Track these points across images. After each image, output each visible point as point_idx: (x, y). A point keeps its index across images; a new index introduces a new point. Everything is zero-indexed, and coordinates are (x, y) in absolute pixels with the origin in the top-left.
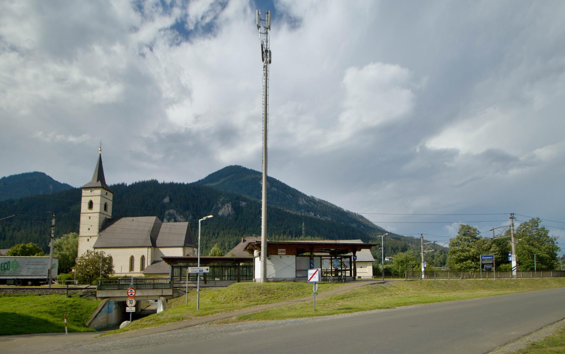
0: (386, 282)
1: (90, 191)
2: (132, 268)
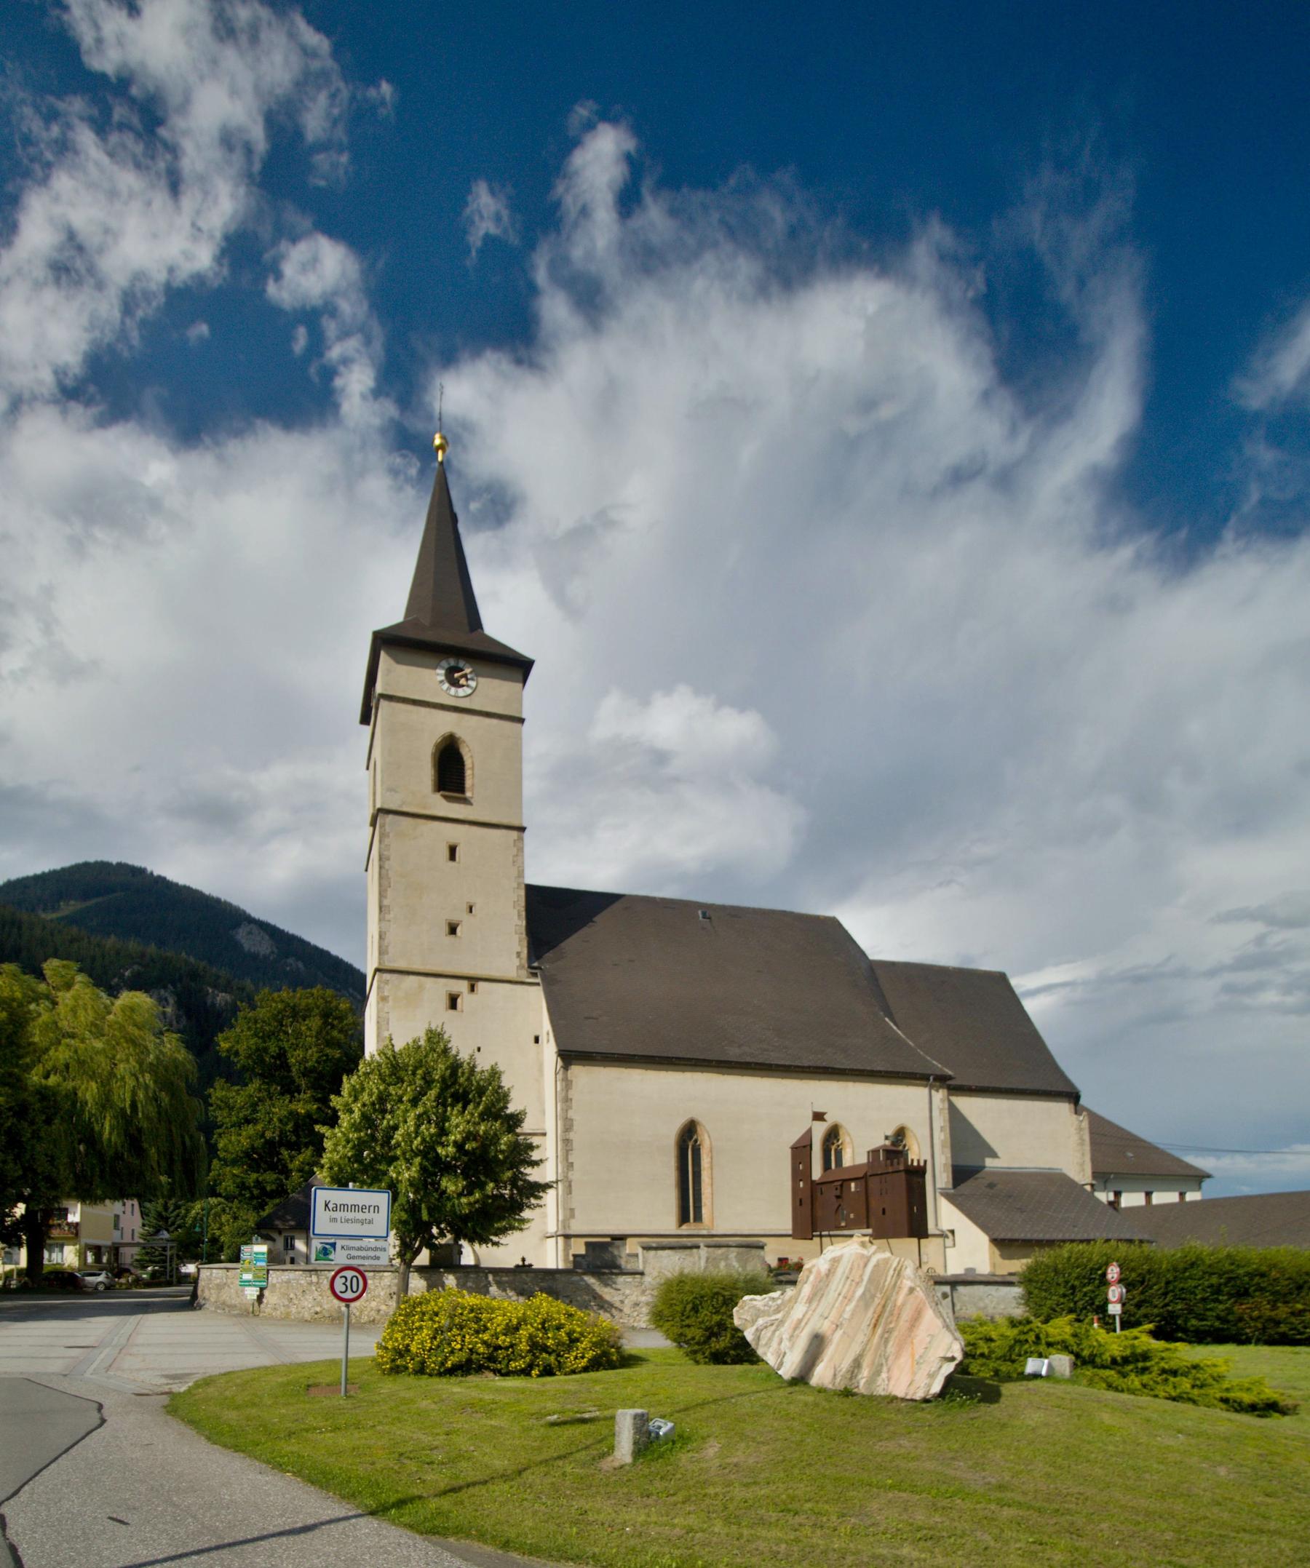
0: (901, 1270)
1: (440, 674)
2: (133, 1238)
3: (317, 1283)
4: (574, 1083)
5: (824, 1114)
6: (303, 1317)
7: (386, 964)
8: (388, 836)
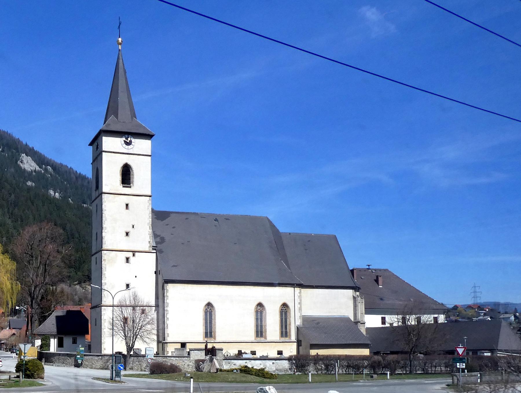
4: (169, 290)
7: (105, 248)
8: (106, 202)
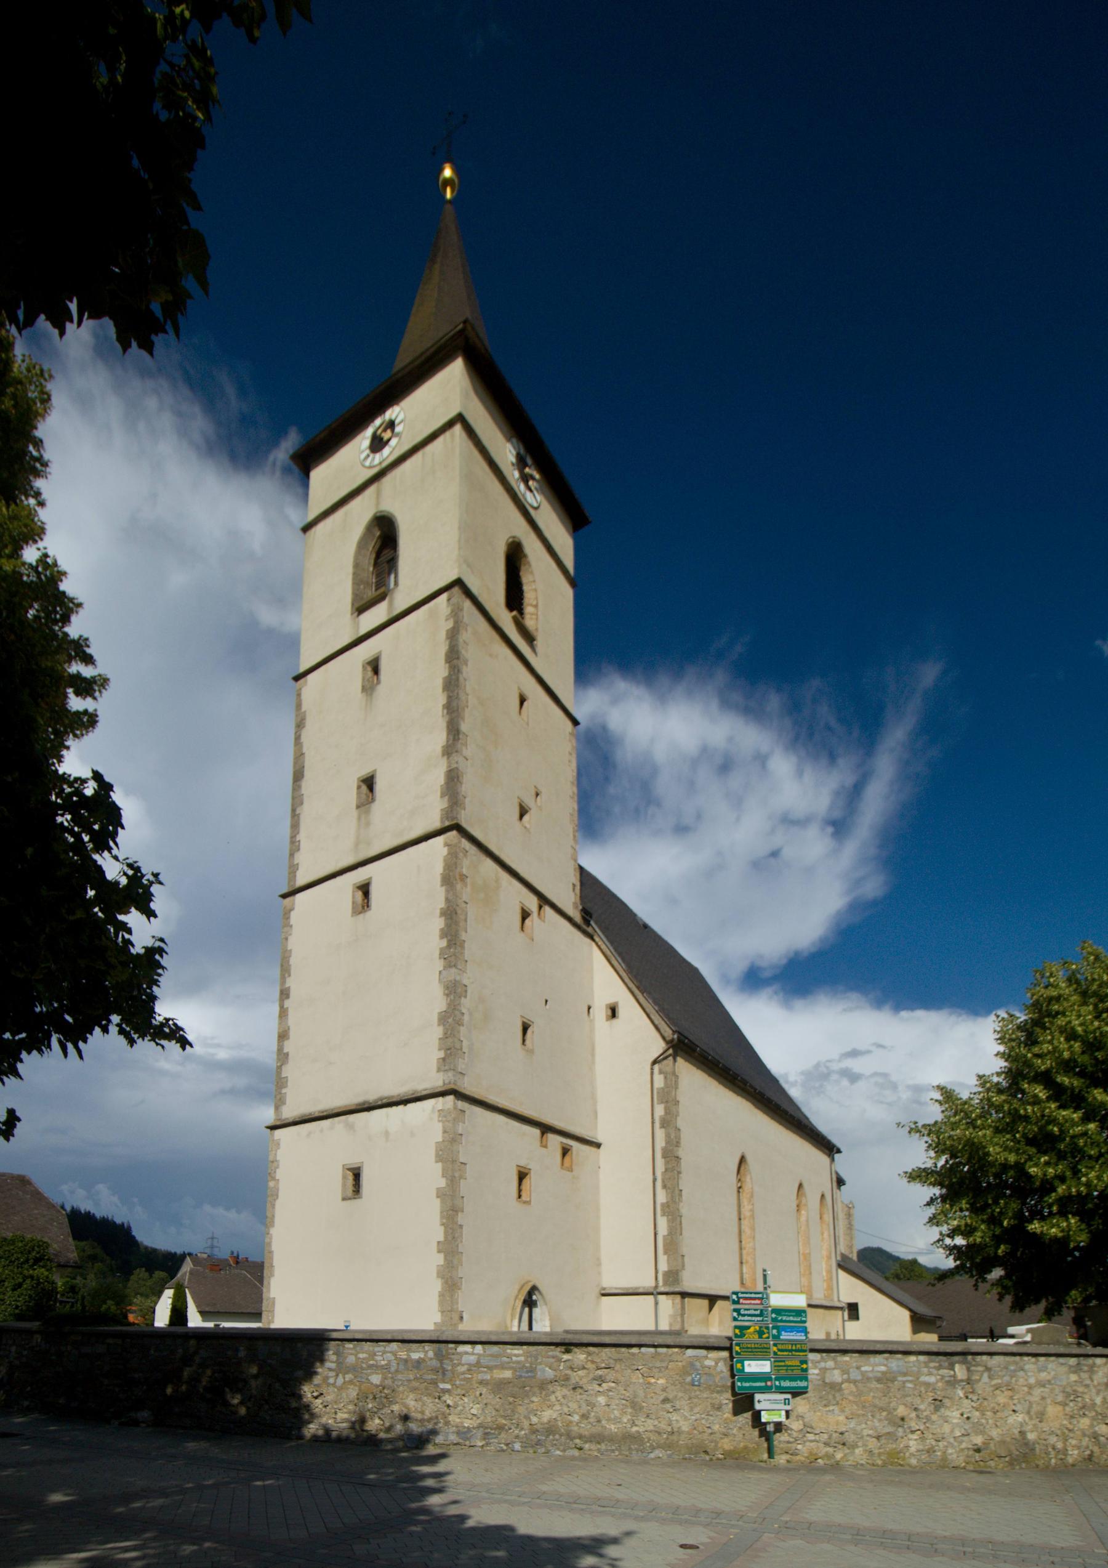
3: (969, 1381)
5: (839, 1151)
6: (944, 1459)
